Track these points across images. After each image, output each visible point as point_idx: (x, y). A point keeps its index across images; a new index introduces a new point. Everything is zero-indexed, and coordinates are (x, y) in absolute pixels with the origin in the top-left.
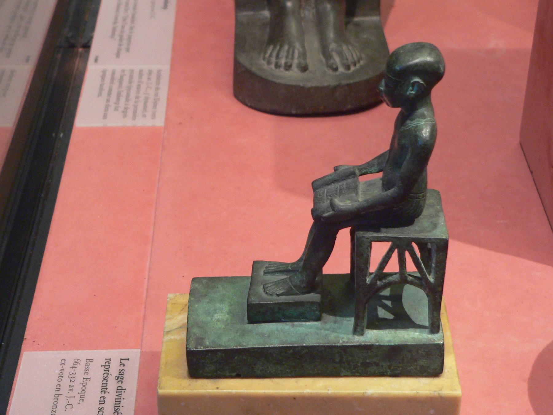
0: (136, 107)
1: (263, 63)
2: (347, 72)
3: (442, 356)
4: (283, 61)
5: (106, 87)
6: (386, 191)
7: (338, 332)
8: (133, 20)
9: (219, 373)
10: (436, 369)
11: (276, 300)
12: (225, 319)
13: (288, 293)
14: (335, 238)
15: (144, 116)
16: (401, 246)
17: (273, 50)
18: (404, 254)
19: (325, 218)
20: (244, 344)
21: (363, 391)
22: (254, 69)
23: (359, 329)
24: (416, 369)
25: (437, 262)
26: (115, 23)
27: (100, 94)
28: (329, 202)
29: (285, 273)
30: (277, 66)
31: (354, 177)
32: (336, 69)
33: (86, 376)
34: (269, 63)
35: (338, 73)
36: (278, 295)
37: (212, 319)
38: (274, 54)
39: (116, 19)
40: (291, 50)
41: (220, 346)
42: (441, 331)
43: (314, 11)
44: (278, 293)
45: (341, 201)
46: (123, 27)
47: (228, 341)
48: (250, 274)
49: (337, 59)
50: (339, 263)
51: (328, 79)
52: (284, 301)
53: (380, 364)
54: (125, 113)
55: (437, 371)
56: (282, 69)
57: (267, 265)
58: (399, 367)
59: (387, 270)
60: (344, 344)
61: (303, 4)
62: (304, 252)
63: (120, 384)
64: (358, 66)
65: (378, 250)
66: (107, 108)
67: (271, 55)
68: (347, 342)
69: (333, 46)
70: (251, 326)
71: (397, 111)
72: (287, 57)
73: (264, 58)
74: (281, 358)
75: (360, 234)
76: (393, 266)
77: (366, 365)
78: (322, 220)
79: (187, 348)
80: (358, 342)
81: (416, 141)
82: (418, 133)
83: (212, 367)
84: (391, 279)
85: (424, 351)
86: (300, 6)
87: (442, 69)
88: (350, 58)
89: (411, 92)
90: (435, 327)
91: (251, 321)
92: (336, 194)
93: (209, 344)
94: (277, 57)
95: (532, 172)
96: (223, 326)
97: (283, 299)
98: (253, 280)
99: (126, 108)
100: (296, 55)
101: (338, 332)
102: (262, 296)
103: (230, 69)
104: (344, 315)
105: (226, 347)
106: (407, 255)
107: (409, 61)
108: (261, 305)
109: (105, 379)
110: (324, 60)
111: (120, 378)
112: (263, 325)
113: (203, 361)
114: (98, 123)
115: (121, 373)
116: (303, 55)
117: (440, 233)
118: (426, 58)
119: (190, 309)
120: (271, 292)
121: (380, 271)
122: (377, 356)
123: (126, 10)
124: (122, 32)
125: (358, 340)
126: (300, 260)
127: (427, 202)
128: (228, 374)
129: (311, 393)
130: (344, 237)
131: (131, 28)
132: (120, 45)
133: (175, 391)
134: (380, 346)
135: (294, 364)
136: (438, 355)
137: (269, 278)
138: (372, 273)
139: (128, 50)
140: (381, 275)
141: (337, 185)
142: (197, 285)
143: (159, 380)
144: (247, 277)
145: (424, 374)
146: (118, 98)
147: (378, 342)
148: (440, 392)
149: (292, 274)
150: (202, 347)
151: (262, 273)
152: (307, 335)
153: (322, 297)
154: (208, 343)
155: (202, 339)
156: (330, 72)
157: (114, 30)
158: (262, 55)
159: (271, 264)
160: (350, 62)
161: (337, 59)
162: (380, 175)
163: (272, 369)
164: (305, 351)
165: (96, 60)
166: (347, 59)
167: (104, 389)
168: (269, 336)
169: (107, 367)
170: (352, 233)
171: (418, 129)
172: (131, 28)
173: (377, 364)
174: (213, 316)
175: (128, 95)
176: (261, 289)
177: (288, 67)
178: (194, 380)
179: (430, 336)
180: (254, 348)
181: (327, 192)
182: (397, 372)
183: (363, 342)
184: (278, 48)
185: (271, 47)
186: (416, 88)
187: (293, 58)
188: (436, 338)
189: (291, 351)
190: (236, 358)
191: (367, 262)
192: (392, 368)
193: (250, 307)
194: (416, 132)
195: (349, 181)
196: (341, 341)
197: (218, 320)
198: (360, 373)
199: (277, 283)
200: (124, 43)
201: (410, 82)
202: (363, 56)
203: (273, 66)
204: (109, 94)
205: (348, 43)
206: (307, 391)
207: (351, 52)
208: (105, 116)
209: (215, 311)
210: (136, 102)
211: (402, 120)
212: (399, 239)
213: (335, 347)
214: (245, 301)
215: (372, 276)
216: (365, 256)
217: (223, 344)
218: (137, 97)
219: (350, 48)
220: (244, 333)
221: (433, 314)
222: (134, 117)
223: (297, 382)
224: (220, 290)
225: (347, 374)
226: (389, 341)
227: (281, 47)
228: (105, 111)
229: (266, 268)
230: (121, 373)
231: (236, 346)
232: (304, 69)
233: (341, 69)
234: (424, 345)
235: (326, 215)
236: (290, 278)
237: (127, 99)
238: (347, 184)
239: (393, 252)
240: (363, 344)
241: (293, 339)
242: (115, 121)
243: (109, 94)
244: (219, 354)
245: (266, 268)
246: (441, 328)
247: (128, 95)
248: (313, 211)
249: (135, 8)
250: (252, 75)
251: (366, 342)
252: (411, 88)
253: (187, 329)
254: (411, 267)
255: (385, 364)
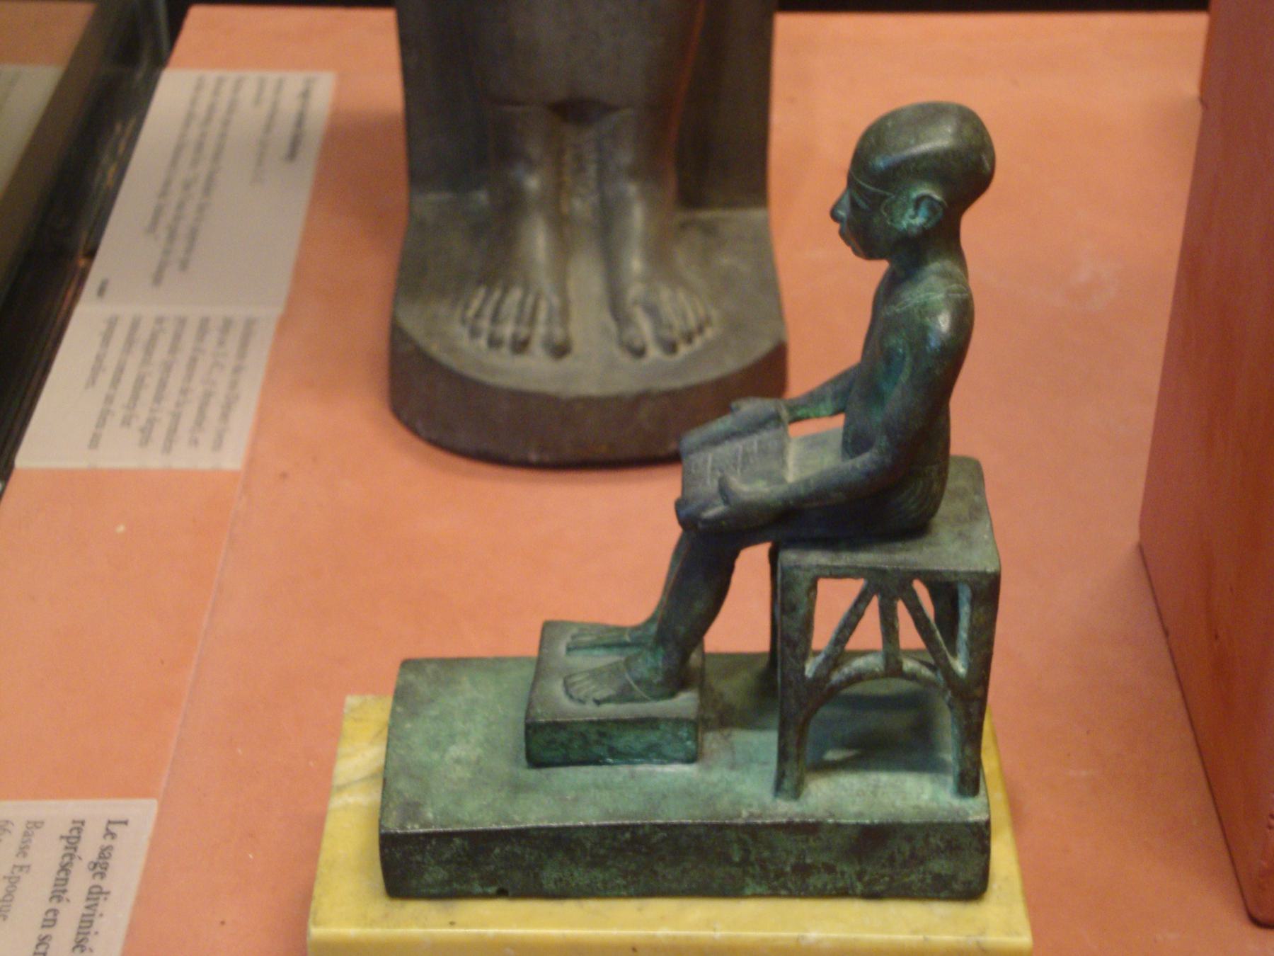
0: (176, 417)
1: (460, 333)
2: (668, 359)
3: (985, 851)
4: (507, 330)
5: (111, 363)
6: (852, 457)
7: (737, 779)
8: (207, 190)
9: (455, 885)
10: (970, 883)
11: (591, 711)
12: (473, 758)
13: (624, 696)
14: (730, 569)
15: (195, 442)
16: (887, 589)
17: (485, 301)
18: (894, 608)
19: (706, 521)
20: (517, 818)
21: (796, 934)
22: (435, 349)
23: (787, 784)
24: (922, 881)
25: (973, 629)
26: (164, 193)
27: (92, 381)
28: (716, 483)
29: (616, 650)
30: (494, 343)
31: (777, 426)
32: (639, 353)
33: (21, 861)
34: (474, 333)
35: (645, 362)
36: (598, 702)
37: (442, 757)
38: (488, 311)
39: (167, 184)
40: (530, 300)
41: (458, 822)
42: (982, 792)
43: (594, 199)
44: (598, 695)
45: (746, 481)
46: (181, 206)
47: (479, 811)
48: (532, 650)
49: (644, 328)
50: (742, 624)
51: (625, 378)
52: (612, 717)
53: (838, 869)
54: (146, 435)
55: (973, 889)
56: (505, 350)
57: (575, 631)
58: (883, 876)
59: (852, 645)
60: (751, 821)
61: (568, 179)
62: (661, 603)
63: (97, 881)
64: (698, 342)
65: (833, 599)
66: (102, 420)
67: (478, 315)
68: (760, 816)
69: (635, 291)
70: (533, 774)
71: (880, 267)
72: (518, 321)
73: (463, 321)
74: (602, 852)
75: (789, 557)
76: (868, 634)
77: (803, 870)
78: (700, 526)
79: (381, 826)
80: (784, 815)
81: (925, 339)
82: (928, 319)
83: (441, 874)
84: (859, 663)
85: (941, 839)
86: (559, 186)
87: (987, 165)
88: (677, 323)
89: (913, 220)
90: (969, 783)
91: (535, 761)
92: (735, 465)
93: (432, 818)
94: (496, 318)
95: (1167, 633)
96: (468, 775)
97: (610, 710)
98: (541, 668)
99: (151, 422)
100: (542, 315)
101: (737, 779)
102: (561, 703)
103: (382, 346)
104: (763, 728)
105: (473, 824)
106: (901, 608)
107: (907, 146)
108: (557, 726)
109: (64, 868)
110: (612, 326)
111: (100, 866)
112: (563, 771)
113: (419, 858)
114: (76, 459)
115: (105, 853)
116: (564, 313)
117: (977, 560)
118: (940, 139)
119: (394, 735)
120: (582, 694)
121: (838, 648)
122: (829, 848)
123: (195, 163)
124: (177, 218)
125: (785, 809)
126: (651, 620)
127: (950, 485)
128: (478, 889)
129: (675, 938)
130: (752, 564)
131: (201, 208)
132: (167, 252)
133: (351, 931)
134: (838, 826)
135: (633, 867)
136: (977, 850)
137: (582, 661)
138: (816, 653)
139: (184, 265)
140: (838, 653)
141: (738, 445)
142: (411, 677)
143: (314, 904)
144: (528, 659)
145: (942, 895)
146: (135, 397)
147: (832, 815)
148: (982, 939)
149: (631, 652)
150: (417, 826)
151: (562, 648)
152: (664, 797)
153: (702, 707)
154: (430, 815)
155: (417, 805)
156: (625, 359)
157: (158, 213)
158: (458, 312)
159: (584, 628)
160: (675, 335)
161: (644, 328)
162: (840, 420)
163: (580, 876)
164: (663, 834)
165: (101, 291)
166: (670, 327)
167: (59, 893)
168: (576, 800)
169: (72, 841)
170: (773, 557)
171: (926, 310)
172: (201, 208)
173: (830, 869)
174: (445, 751)
175: (162, 384)
176: (557, 688)
177: (520, 346)
178: (398, 903)
179: (957, 803)
180: (539, 829)
181: (714, 461)
182: (878, 888)
183: (797, 815)
184: (497, 294)
185: (481, 292)
186: (923, 211)
187: (532, 320)
188: (972, 809)
189: (628, 835)
190: (497, 851)
191: (807, 626)
192: (866, 878)
193: (532, 729)
194: (922, 317)
195: (766, 435)
196: (745, 813)
197: (458, 761)
198: (789, 890)
199: (594, 674)
200: (179, 244)
201: (908, 196)
202: (714, 313)
203: (483, 342)
204: (116, 381)
205: (676, 280)
206: (663, 932)
207: (681, 307)
208: (95, 442)
209: (452, 739)
210: (178, 405)
211: (889, 289)
212: (882, 572)
213: (729, 826)
214: (522, 715)
215: (820, 659)
216: (802, 612)
217: (467, 819)
218: (184, 392)
219: (681, 295)
220: (517, 788)
221: (963, 751)
222: (168, 448)
223: (640, 910)
224: (468, 689)
225: (759, 890)
226: (860, 815)
227: (506, 290)
228: (97, 426)
229: (573, 637)
230: (105, 853)
231: (497, 824)
232: (560, 350)
233: (654, 353)
234: (940, 824)
235: (710, 513)
236: (627, 663)
237: (158, 398)
238: (760, 442)
239: (868, 602)
240: (797, 820)
241: (633, 807)
242: (122, 453)
243: (116, 381)
244: (457, 841)
245: (573, 637)
246: (981, 783)
247: (162, 384)
248: (679, 505)
249: (217, 156)
250: (429, 363)
251: (803, 815)
252: (911, 211)
253: (385, 781)
254: (909, 637)
255: (849, 869)
